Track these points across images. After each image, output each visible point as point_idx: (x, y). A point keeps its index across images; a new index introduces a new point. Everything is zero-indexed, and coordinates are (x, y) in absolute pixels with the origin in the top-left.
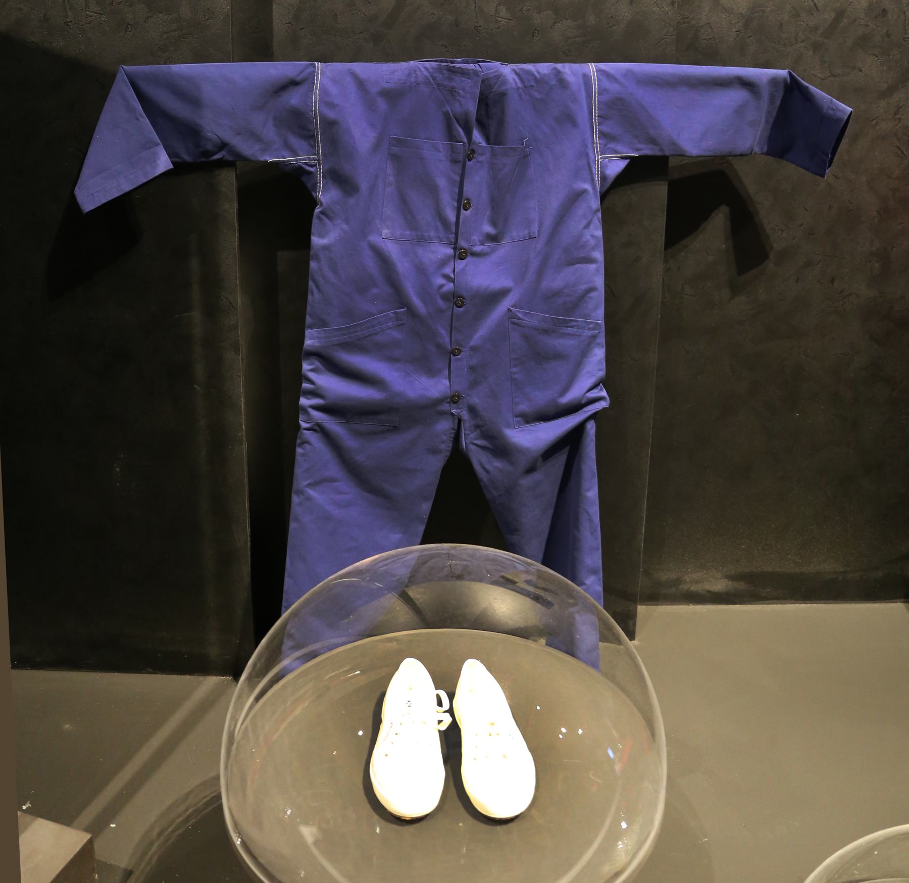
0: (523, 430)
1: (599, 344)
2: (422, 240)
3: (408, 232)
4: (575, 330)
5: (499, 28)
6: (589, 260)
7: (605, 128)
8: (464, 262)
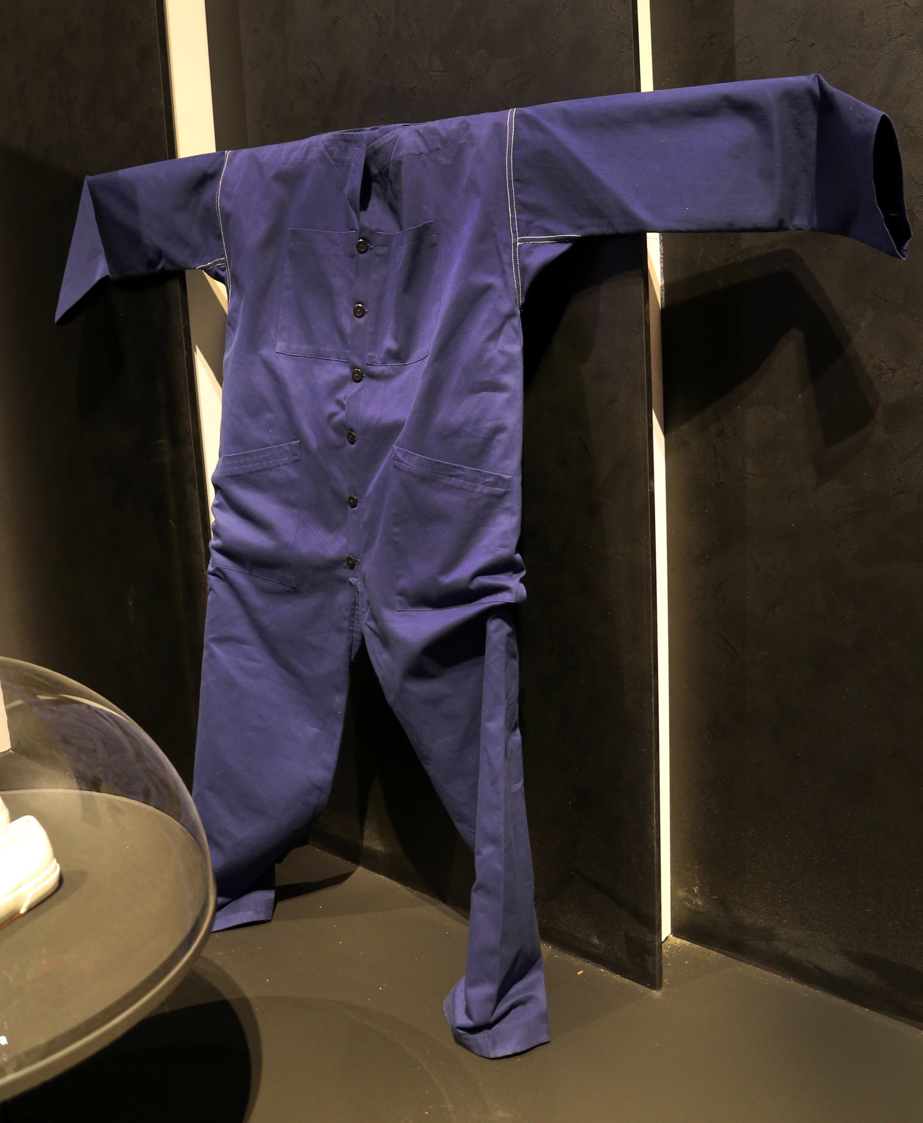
0: (405, 615)
1: (507, 510)
2: (319, 357)
3: (304, 347)
4: (461, 481)
5: (433, 86)
6: (498, 387)
7: (525, 198)
8: (359, 385)
